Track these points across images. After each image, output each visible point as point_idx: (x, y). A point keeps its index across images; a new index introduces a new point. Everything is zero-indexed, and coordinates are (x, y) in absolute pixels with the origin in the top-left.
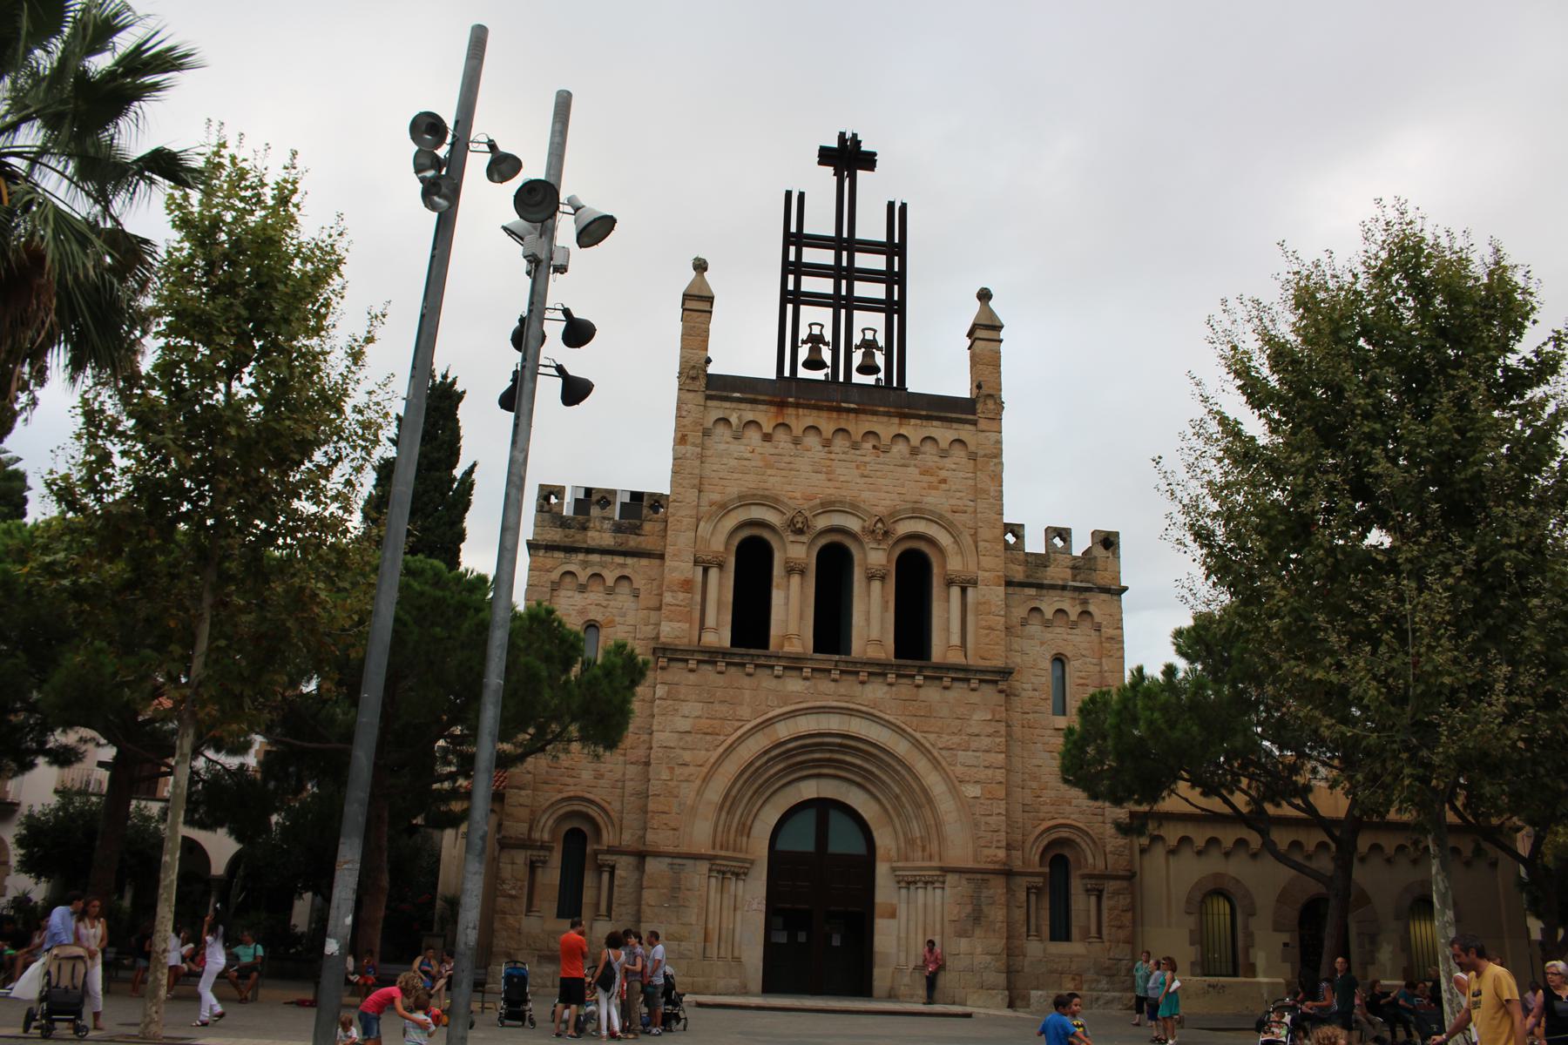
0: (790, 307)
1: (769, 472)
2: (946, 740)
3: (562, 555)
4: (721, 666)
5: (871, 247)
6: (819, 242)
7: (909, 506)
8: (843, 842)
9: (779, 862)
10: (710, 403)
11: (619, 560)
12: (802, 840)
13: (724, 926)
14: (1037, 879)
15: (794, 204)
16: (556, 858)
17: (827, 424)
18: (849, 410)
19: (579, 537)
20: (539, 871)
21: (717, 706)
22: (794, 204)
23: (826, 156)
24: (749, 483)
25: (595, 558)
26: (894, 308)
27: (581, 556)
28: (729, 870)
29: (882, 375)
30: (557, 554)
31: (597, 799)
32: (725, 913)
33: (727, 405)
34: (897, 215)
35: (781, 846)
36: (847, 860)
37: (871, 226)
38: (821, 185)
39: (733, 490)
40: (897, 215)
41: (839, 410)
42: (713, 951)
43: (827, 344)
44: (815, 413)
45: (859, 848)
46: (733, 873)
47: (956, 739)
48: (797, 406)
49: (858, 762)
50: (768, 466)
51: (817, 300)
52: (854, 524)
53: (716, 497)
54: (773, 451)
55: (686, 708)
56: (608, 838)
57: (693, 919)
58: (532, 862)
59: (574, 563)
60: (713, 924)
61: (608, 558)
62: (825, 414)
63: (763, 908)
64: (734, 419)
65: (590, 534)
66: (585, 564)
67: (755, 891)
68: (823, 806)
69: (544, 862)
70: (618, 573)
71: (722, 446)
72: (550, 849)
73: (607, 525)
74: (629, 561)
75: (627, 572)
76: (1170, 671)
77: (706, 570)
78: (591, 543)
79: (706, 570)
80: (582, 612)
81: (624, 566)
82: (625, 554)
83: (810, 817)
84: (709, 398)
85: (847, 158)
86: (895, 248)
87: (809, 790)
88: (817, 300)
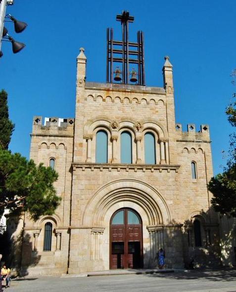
1: (105, 110)
2: (163, 188)
3: (41, 137)
8: (132, 220)
9: (113, 229)
10: (86, 90)
11: (60, 138)
12: (119, 221)
15: (110, 33)
16: (42, 233)
19: (47, 132)
20: (36, 237)
22: (110, 33)
24: (100, 113)
25: (53, 138)
27: (48, 138)
28: (97, 231)
33: (92, 91)
34: (140, 36)
35: (113, 223)
36: (133, 227)
37: (133, 39)
38: (118, 27)
39: (94, 116)
40: (140, 36)
44: (118, 92)
50: (105, 109)
52: (131, 125)
53: (89, 118)
55: (83, 182)
58: (34, 234)
59: (46, 140)
61: (56, 138)
62: (121, 93)
63: (109, 243)
67: (105, 239)
70: (51, 142)
74: (63, 138)
77: (87, 141)
78: (51, 134)
79: (87, 141)
80: (49, 155)
83: (122, 213)
84: (86, 89)
85: (125, 18)
86: (140, 45)
87: (122, 205)
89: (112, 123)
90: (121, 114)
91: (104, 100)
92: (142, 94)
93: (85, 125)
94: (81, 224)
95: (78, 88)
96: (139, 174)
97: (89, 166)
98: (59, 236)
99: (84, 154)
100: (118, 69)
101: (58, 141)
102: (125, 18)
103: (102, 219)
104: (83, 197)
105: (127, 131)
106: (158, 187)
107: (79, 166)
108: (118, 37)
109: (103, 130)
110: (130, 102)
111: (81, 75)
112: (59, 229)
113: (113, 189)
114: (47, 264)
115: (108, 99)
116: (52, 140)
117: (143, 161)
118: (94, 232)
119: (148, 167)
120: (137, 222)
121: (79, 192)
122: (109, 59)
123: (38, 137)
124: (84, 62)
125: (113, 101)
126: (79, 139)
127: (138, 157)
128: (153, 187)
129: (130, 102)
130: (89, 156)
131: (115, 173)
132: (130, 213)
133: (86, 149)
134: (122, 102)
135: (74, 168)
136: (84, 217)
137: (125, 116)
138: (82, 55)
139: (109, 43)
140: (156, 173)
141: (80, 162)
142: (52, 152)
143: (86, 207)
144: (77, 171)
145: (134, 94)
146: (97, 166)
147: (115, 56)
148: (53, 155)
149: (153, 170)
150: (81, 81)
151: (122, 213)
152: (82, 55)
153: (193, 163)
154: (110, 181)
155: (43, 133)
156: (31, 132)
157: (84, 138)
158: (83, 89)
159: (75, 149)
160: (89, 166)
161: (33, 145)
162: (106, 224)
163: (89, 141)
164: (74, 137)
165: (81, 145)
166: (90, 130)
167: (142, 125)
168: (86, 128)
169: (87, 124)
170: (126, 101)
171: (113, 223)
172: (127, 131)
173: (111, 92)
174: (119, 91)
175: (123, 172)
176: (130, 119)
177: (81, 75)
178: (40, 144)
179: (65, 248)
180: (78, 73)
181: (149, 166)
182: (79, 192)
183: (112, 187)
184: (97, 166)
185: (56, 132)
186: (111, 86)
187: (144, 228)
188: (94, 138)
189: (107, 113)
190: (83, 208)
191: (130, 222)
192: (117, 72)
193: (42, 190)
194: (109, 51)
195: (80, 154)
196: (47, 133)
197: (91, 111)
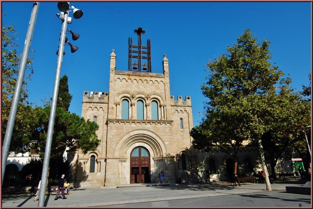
1: (128, 87)
2: (163, 134)
3: (89, 104)
8: (144, 154)
9: (132, 159)
10: (116, 75)
11: (100, 104)
12: (136, 154)
15: (130, 41)
16: (89, 162)
17: (149, 79)
20: (85, 164)
22: (130, 41)
24: (124, 89)
25: (95, 104)
27: (93, 104)
28: (122, 160)
32: (122, 169)
33: (119, 75)
34: (149, 42)
35: (132, 156)
36: (144, 158)
38: (135, 37)
39: (121, 91)
40: (149, 42)
50: (127, 86)
51: (134, 57)
52: (143, 96)
53: (118, 92)
55: (114, 131)
58: (84, 162)
59: (91, 105)
61: (98, 104)
62: (137, 77)
77: (116, 106)
78: (94, 101)
79: (116, 106)
80: (93, 114)
82: (101, 103)
83: (138, 149)
84: (116, 74)
85: (139, 32)
86: (149, 48)
87: (138, 144)
88: (134, 57)
89: (132, 95)
90: (137, 90)
91: (127, 81)
92: (150, 78)
93: (115, 96)
94: (113, 156)
95: (111, 74)
96: (148, 126)
97: (118, 121)
98: (99, 164)
99: (115, 113)
100: (135, 62)
101: (99, 106)
103: (126, 153)
104: (114, 140)
105: (141, 100)
107: (112, 121)
108: (135, 43)
109: (126, 99)
110: (143, 82)
111: (113, 66)
114: (92, 181)
115: (129, 81)
117: (150, 118)
118: (121, 161)
119: (153, 122)
120: (147, 155)
122: (130, 57)
123: (86, 103)
124: (115, 58)
125: (132, 82)
126: (111, 105)
127: (148, 116)
128: (157, 133)
129: (143, 82)
130: (118, 115)
131: (133, 125)
133: (115, 111)
134: (138, 82)
135: (109, 122)
136: (115, 152)
138: (113, 54)
139: (130, 46)
140: (158, 125)
141: (112, 119)
142: (95, 112)
143: (116, 146)
144: (110, 124)
146: (122, 121)
147: (133, 54)
150: (113, 70)
151: (138, 149)
152: (113, 54)
154: (131, 130)
155: (90, 101)
157: (114, 104)
159: (109, 110)
160: (118, 121)
161: (83, 108)
162: (128, 156)
163: (118, 106)
164: (108, 103)
165: (113, 108)
166: (118, 99)
168: (116, 98)
169: (116, 96)
170: (140, 82)
171: (132, 156)
172: (141, 100)
174: (136, 76)
177: (113, 66)
178: (87, 108)
179: (103, 170)
182: (111, 137)
183: (132, 134)
184: (122, 121)
185: (98, 101)
186: (131, 73)
187: (151, 158)
188: (121, 104)
189: (128, 89)
190: (114, 146)
191: (142, 155)
194: (130, 51)
196: (92, 101)
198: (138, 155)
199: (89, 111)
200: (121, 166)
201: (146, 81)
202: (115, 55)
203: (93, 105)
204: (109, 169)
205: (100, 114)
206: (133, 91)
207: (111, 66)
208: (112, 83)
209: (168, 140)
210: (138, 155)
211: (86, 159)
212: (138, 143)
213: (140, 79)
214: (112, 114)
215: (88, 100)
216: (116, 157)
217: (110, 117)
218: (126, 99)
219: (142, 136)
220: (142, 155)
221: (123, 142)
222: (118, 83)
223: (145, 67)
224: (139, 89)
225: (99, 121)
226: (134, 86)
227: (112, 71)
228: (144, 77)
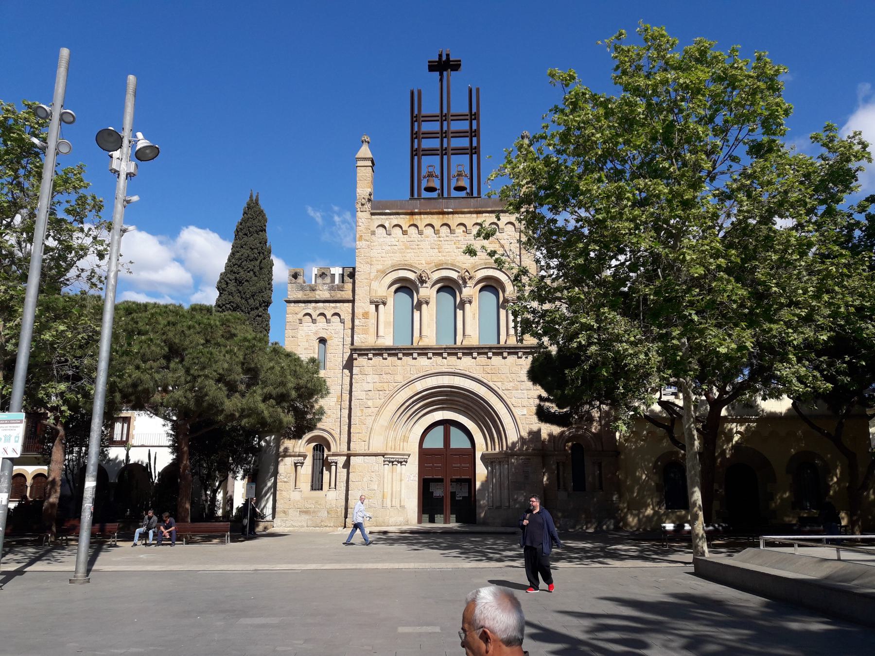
0: (474, 110)
1: (408, 251)
2: (510, 385)
3: (303, 305)
4: (385, 356)
5: (459, 117)
6: (430, 118)
7: (482, 262)
8: (458, 441)
9: (425, 455)
10: (373, 217)
11: (332, 305)
12: (435, 441)
13: (394, 490)
14: (114, 559)
15: (415, 98)
16: (309, 461)
17: (436, 220)
18: (448, 213)
19: (311, 295)
20: (299, 468)
21: (384, 376)
22: (415, 98)
23: (432, 67)
24: (397, 259)
26: (473, 151)
27: (313, 304)
28: (396, 460)
29: (468, 190)
30: (301, 305)
31: (327, 429)
35: (424, 446)
36: (460, 452)
37: (460, 106)
39: (389, 263)
41: (443, 213)
42: (388, 503)
43: (437, 177)
45: (468, 445)
46: (398, 462)
47: (512, 384)
48: (420, 213)
49: (461, 400)
50: (407, 248)
52: (454, 275)
53: (380, 267)
54: (409, 239)
55: (369, 378)
56: (334, 449)
57: (376, 487)
58: (295, 464)
59: (310, 308)
60: (388, 489)
61: (327, 304)
62: (435, 216)
64: (387, 225)
65: (317, 292)
66: (315, 308)
67: (410, 473)
68: (447, 424)
69: (303, 463)
70: (333, 312)
71: (382, 240)
72: (305, 457)
73: (326, 287)
74: (338, 305)
75: (337, 311)
76: (243, 478)
77: (377, 307)
78: (318, 298)
79: (377, 307)
80: (316, 333)
81: (335, 308)
83: (440, 429)
84: (372, 214)
86: (473, 116)
89: (419, 272)
90: (437, 257)
91: (405, 233)
92: (475, 215)
93: (373, 283)
94: (366, 448)
95: (359, 214)
96: (466, 363)
97: (379, 352)
98: (333, 468)
99: (373, 330)
100: (431, 169)
101: (329, 309)
102: (443, 66)
103: (405, 439)
104: (370, 403)
105: (449, 287)
106: (499, 384)
107: (363, 352)
108: (430, 107)
109: (405, 287)
110: (452, 232)
111: (364, 189)
112: (333, 455)
113: (420, 389)
114: (314, 512)
115: (413, 230)
116: (319, 308)
117: (473, 340)
118: (390, 462)
119: (482, 351)
120: (468, 445)
121: (363, 395)
122: (415, 153)
123: (297, 305)
124: (369, 163)
125: (420, 233)
126: (363, 305)
127: (466, 333)
128: (491, 384)
129: (452, 232)
130: (381, 333)
131: (423, 361)
132: (453, 430)
133: (374, 321)
134: (437, 232)
135: (355, 356)
136: (372, 435)
137: (443, 258)
138: (365, 151)
139: (415, 119)
140: (497, 360)
141: (364, 346)
142: (321, 328)
143: (375, 420)
144: (360, 362)
145: (460, 215)
146: (392, 352)
147: (426, 144)
148: (323, 335)
149: (490, 354)
150: (364, 201)
151: (440, 429)
152: (365, 151)
153: (323, 341)
154: (416, 376)
155: (305, 298)
156: (287, 295)
157: (371, 302)
158: (367, 215)
159: (357, 322)
160: (379, 352)
161: (289, 318)
162: (412, 449)
163: (381, 307)
164: (353, 301)
165: (366, 315)
166: (382, 288)
167: (472, 274)
168: (375, 285)
169: (376, 278)
170: (445, 230)
171: (424, 446)
172: (449, 287)
173: (417, 217)
175: (453, 359)
176: (452, 265)
177: (364, 189)
178: (300, 316)
179: (342, 486)
180: (358, 186)
181: (483, 348)
182: (363, 395)
183: (420, 386)
184: (392, 352)
185: (325, 294)
186: (417, 207)
187: (478, 455)
188: (390, 302)
189: (411, 258)
190: (369, 421)
191: (454, 445)
192: (430, 175)
193: (857, 233)
194: (415, 135)
195: (366, 332)
196: (312, 296)
197: (383, 255)
198: (440, 445)
199: (304, 324)
200: (390, 474)
201: (463, 228)
202: (369, 155)
203: (315, 309)
204: (355, 487)
205: (333, 332)
206: (424, 262)
207: (358, 190)
208: (364, 242)
209: (525, 404)
210: (440, 445)
211: (299, 456)
212: (440, 412)
213: (445, 222)
214: (366, 332)
215: (300, 295)
216: (372, 450)
217: (361, 340)
218: (405, 287)
219: (413, 402)
220: (454, 445)
221: (391, 414)
222: (382, 240)
223: (432, 185)
224: (440, 254)
225: (332, 351)
226: (425, 245)
227: (363, 205)
228: (457, 215)
